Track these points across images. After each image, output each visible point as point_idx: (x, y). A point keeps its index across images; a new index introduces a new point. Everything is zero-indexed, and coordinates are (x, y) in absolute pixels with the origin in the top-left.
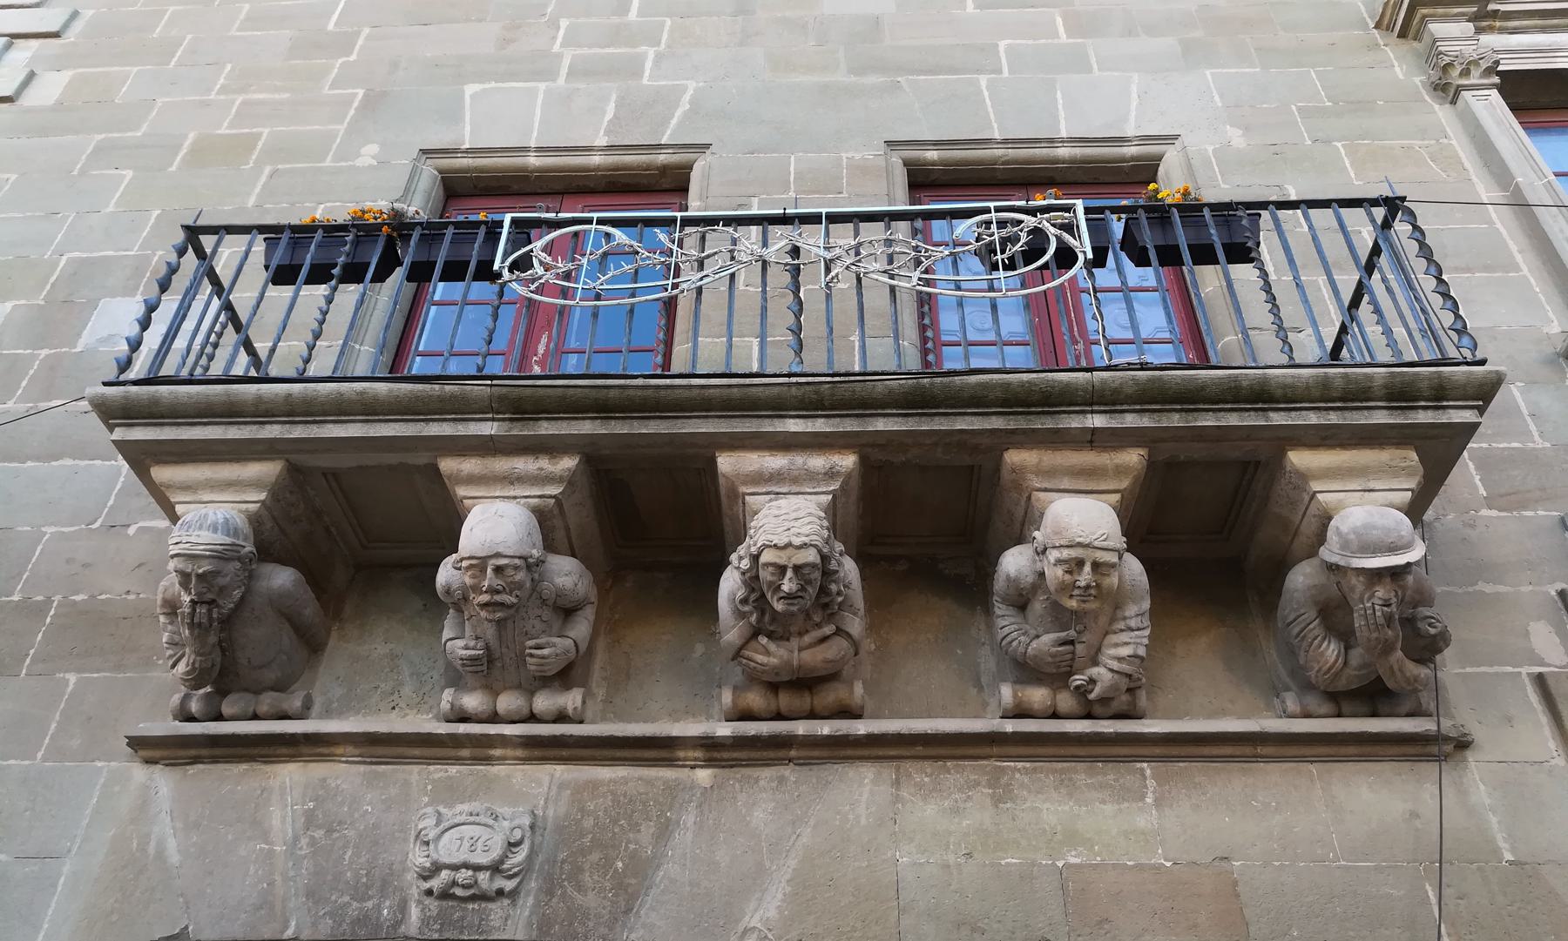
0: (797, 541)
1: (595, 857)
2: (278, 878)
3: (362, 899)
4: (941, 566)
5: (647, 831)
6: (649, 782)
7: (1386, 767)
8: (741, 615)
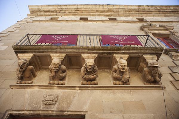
1: (65, 100)
2: (25, 102)
3: (35, 105)
5: (72, 98)
6: (72, 92)
7: (157, 90)
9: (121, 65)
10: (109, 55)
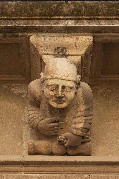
9: (48, 86)
10: (14, 39)
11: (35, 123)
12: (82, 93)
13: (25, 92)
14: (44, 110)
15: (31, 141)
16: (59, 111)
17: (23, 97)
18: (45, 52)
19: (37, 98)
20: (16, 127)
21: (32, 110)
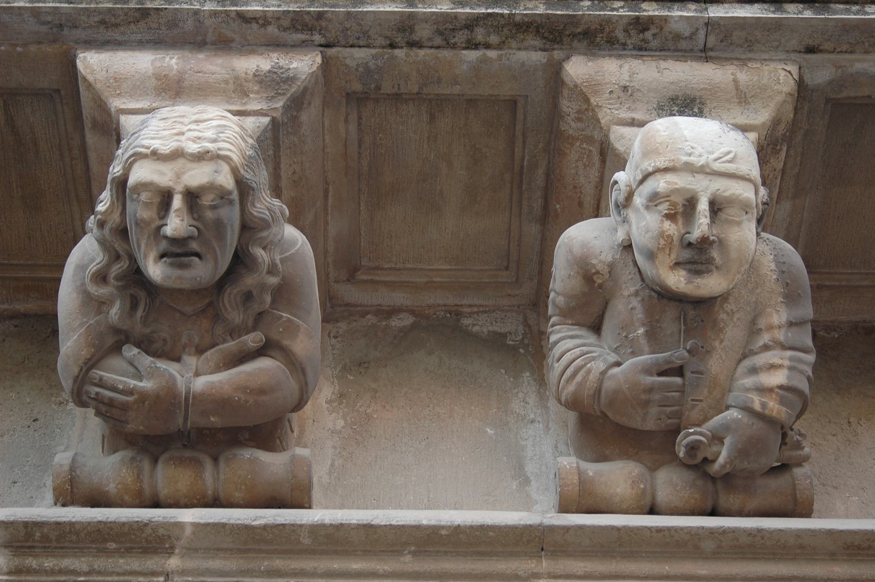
0: (193, 148)
4: (466, 321)
8: (99, 305)
11: (591, 377)
12: (772, 257)
13: (516, 330)
14: (626, 326)
15: (569, 462)
16: (683, 327)
17: (511, 343)
18: (625, 115)
19: (598, 272)
20: (495, 434)
21: (572, 337)
